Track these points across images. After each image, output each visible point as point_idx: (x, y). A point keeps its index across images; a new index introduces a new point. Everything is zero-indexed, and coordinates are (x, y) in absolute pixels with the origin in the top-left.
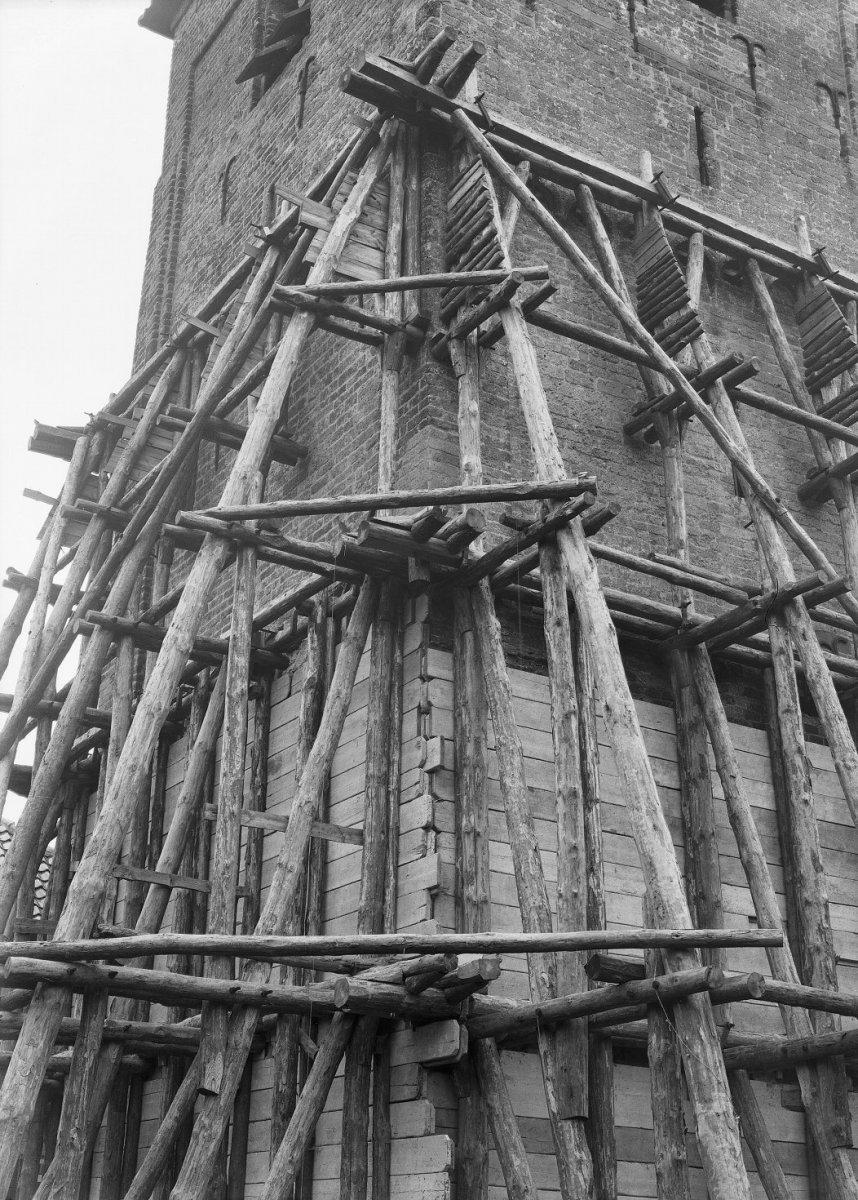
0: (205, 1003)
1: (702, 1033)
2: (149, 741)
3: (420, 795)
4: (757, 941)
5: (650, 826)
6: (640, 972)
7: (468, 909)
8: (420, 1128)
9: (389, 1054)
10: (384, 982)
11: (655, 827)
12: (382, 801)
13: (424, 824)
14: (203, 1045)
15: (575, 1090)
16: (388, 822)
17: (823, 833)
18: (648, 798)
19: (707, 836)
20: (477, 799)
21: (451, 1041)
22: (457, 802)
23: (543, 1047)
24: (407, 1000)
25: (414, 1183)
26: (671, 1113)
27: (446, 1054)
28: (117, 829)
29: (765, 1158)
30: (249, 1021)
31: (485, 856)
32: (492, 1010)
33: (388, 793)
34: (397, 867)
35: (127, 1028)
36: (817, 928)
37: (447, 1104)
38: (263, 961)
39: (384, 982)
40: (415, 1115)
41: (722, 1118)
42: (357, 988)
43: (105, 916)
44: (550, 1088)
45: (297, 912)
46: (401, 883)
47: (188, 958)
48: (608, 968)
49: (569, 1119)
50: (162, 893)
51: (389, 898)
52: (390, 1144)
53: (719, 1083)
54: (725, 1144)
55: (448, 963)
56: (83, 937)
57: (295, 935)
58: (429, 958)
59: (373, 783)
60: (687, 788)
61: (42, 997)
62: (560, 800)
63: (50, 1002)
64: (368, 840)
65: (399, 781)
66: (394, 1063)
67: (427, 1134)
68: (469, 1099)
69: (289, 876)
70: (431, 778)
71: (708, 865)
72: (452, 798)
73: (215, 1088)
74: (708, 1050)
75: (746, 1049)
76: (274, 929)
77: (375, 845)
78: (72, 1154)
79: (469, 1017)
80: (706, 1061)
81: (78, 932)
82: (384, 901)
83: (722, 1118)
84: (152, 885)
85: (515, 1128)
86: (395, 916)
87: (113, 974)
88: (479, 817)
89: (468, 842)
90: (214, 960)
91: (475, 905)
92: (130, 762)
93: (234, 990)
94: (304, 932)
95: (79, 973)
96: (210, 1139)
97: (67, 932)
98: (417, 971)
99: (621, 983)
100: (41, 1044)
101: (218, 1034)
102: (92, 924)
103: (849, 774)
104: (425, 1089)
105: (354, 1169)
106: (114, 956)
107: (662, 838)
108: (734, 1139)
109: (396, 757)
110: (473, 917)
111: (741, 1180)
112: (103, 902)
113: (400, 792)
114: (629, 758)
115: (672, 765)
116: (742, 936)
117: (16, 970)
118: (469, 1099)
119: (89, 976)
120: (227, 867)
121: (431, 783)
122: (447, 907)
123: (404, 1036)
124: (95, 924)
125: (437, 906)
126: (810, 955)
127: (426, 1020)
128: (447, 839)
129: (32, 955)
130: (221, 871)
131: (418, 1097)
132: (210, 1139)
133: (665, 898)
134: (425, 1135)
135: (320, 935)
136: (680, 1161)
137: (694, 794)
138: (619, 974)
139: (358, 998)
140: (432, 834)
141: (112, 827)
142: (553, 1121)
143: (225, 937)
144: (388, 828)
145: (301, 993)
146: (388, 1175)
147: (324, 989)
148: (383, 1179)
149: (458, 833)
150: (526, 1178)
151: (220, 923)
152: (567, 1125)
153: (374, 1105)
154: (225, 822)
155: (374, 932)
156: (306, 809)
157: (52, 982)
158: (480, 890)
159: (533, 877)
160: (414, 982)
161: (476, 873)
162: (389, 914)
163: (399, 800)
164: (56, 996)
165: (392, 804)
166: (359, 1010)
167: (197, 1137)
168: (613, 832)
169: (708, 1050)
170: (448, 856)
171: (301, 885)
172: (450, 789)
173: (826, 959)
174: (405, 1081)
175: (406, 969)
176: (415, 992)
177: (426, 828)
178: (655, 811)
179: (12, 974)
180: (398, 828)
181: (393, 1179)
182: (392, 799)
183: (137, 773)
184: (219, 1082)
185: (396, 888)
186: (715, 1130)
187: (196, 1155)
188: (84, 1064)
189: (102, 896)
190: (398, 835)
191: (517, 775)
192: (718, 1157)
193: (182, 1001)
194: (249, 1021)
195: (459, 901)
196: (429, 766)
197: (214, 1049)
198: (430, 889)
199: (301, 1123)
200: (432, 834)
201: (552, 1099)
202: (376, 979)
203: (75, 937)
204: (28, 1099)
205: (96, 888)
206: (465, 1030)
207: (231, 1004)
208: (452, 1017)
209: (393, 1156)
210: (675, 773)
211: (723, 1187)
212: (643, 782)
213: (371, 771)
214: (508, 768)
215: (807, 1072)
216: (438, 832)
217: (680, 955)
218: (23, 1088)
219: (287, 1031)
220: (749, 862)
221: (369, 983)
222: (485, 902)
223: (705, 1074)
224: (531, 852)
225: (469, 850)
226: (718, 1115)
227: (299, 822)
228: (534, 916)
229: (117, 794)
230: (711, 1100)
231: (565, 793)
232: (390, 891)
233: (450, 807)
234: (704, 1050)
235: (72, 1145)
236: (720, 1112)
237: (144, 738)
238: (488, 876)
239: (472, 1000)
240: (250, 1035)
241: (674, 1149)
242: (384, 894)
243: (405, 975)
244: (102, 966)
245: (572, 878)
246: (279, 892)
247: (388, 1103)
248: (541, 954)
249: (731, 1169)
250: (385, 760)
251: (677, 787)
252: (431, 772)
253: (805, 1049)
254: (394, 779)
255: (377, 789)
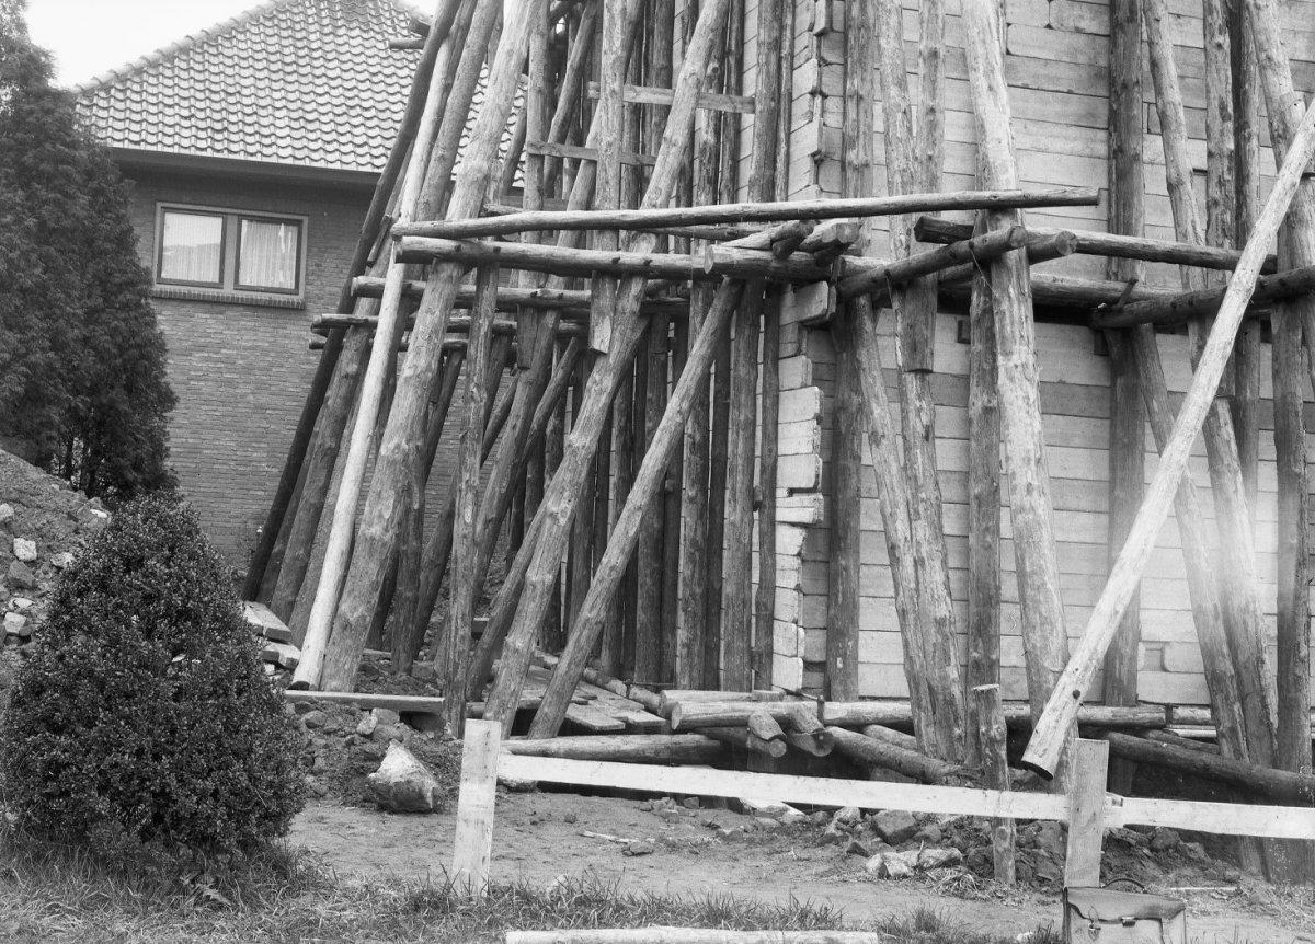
0: (594, 272)
1: (1011, 290)
2: (525, 24)
3: (808, 60)
4: (1071, 200)
5: (986, 87)
6: (966, 232)
7: (850, 174)
8: (798, 381)
9: (779, 315)
10: (750, 248)
11: (990, 88)
12: (773, 67)
13: (810, 90)
14: (593, 307)
15: (919, 345)
16: (779, 90)
17: (1294, 72)
18: (987, 58)
19: (1131, 84)
20: (861, 62)
21: (821, 300)
22: (845, 65)
23: (896, 305)
24: (774, 264)
25: (794, 429)
26: (985, 365)
27: (817, 314)
28: (497, 113)
29: (1156, 409)
30: (636, 287)
31: (869, 120)
32: (857, 271)
33: (780, 60)
34: (789, 134)
35: (561, 297)
36: (1216, 180)
37: (827, 358)
38: (648, 232)
39: (750, 248)
40: (795, 370)
41: (1020, 369)
42: (722, 255)
43: (491, 197)
44: (898, 343)
45: (709, 182)
46: (792, 150)
47: (545, 231)
48: (931, 229)
49: (913, 371)
50: (591, 168)
51: (780, 165)
52: (778, 396)
53: (1022, 337)
54: (1020, 393)
55: (804, 228)
56: (471, 216)
57: (707, 204)
58: (791, 223)
59: (764, 50)
60: (1115, 33)
61: (436, 271)
62: (921, 61)
63: (444, 275)
64: (759, 108)
65: (792, 46)
66: (783, 322)
67: (804, 386)
68: (844, 354)
69: (673, 150)
70: (819, 41)
71: (1128, 116)
72: (841, 61)
73: (604, 348)
74: (1016, 306)
75: (1143, 304)
76: (659, 202)
77: (765, 114)
78: (473, 405)
79: (840, 279)
80: (1012, 316)
81: (466, 212)
82: (775, 169)
83: (1020, 369)
84: (583, 162)
85: (879, 381)
86: (787, 184)
87: (497, 250)
88: (862, 79)
89: (851, 106)
90: (600, 233)
91: (856, 169)
92: (507, 47)
93: (616, 261)
94: (890, 193)
95: (465, 248)
96: (601, 392)
97: (458, 215)
98: (781, 237)
99: (950, 243)
100: (438, 313)
101: (605, 301)
102: (479, 204)
103: (1258, 14)
104: (804, 346)
105: (742, 418)
106: (501, 233)
107: (995, 100)
108: (1029, 388)
109: (789, 21)
110: (854, 182)
111: (1031, 424)
112: (488, 182)
113: (793, 57)
114: (973, 17)
115: (1103, 9)
116: (1056, 196)
117: (407, 248)
118: (844, 354)
119: (475, 252)
120: (610, 145)
121: (819, 47)
122: (831, 173)
123: (789, 298)
124: (482, 206)
125: (821, 172)
126: (386, 237)
127: (804, 281)
128: (833, 104)
129: (425, 235)
130: (604, 148)
131: (798, 353)
132: (601, 392)
133: (991, 160)
134: (802, 387)
135: (733, 202)
136: (990, 408)
137: (1121, 41)
138: (944, 235)
139: (723, 264)
140: (818, 99)
141: (492, 114)
142: (899, 371)
143: (610, 212)
144: (780, 94)
145: (684, 261)
146: (776, 423)
147: (702, 257)
148: (770, 427)
149: (844, 98)
150: (884, 425)
151: (605, 199)
152: (910, 378)
153: (765, 363)
154: (607, 99)
155: (764, 200)
156: (690, 81)
157: (445, 257)
158: (861, 153)
159: (900, 140)
160: (778, 246)
161: (858, 136)
162: (780, 181)
163: (792, 65)
164: (449, 270)
165: (784, 70)
166: (739, 277)
167: (589, 391)
168: (1025, 87)
169: (1016, 306)
170: (833, 120)
171: (713, 156)
172: (839, 52)
173: (1223, 213)
174: (790, 336)
175: (773, 235)
176: (783, 256)
177: (813, 93)
178: (992, 71)
179: (405, 252)
180: (791, 93)
181: (780, 427)
182: (784, 65)
183: (515, 57)
184: (607, 343)
185: (788, 154)
186: (1012, 379)
187: (589, 405)
188: (479, 328)
189: (487, 178)
190: (791, 100)
191: (892, 35)
192: (1011, 405)
193: (574, 272)
194: (636, 287)
195: (843, 165)
196: (817, 29)
197: (602, 314)
198: (813, 155)
199: (690, 377)
200: (818, 99)
201: (899, 353)
202: (746, 248)
203: (463, 216)
204: (429, 359)
205: (479, 171)
206: (834, 291)
207: (615, 273)
208: (821, 280)
209: (781, 407)
210: (1106, 18)
211: (1012, 430)
212: (984, 42)
213: (761, 38)
214: (884, 28)
215: (1196, 328)
216: (825, 96)
217: (999, 216)
218: (424, 349)
219: (700, 296)
220: (1163, 112)
221: (735, 250)
222: (867, 165)
223: (1009, 328)
224: (900, 115)
225: (852, 115)
226: (1016, 366)
227: (684, 95)
228: (898, 178)
229: (496, 80)
230: (1011, 353)
231: (926, 53)
232: (781, 159)
233: (839, 69)
234: (1011, 305)
235: (472, 397)
236: (1019, 363)
237: (520, 22)
238: (871, 139)
239: (844, 261)
240: (637, 300)
241: (985, 398)
242: (775, 161)
243: (773, 241)
244: (490, 243)
245: (928, 140)
246: (663, 167)
247: (777, 359)
248: (901, 216)
249: (1023, 414)
250: (776, 25)
251: (1107, 33)
252: (820, 35)
253: (1191, 303)
254: (786, 44)
255: (768, 56)
